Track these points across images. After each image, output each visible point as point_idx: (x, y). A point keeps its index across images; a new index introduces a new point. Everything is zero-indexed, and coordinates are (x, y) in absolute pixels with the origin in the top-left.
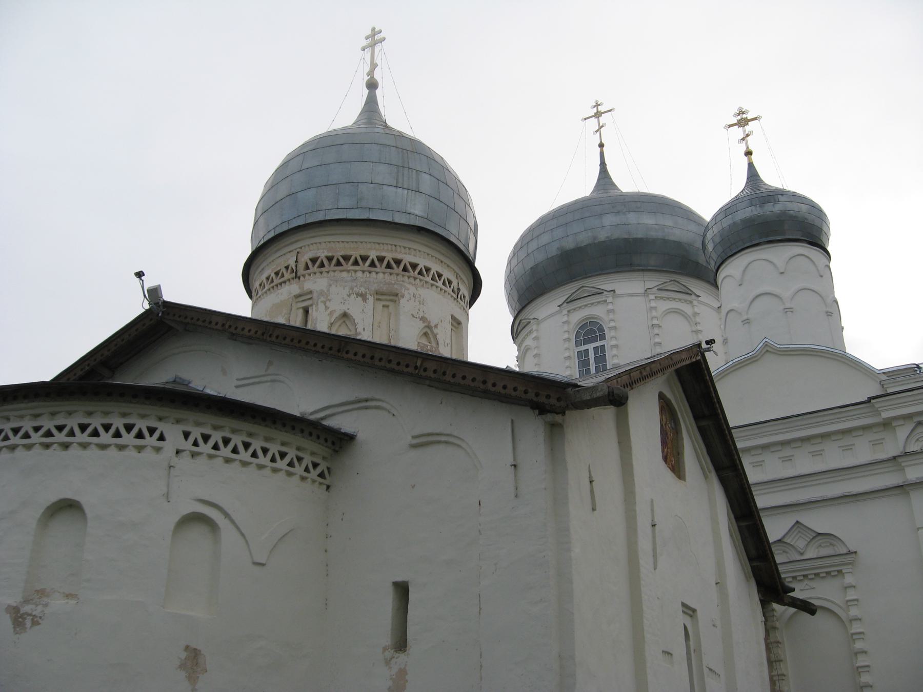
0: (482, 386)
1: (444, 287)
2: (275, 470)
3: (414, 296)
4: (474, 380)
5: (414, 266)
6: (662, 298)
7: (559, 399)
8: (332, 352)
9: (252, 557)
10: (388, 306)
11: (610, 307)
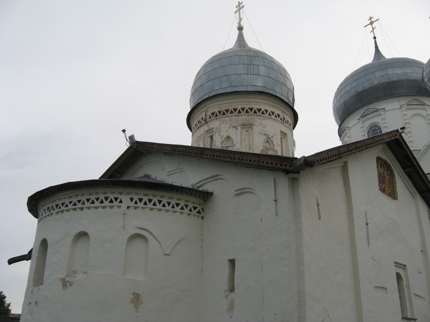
0: (258, 164)
1: (275, 118)
2: (175, 212)
3: (260, 124)
4: (254, 161)
5: (259, 110)
6: (409, 109)
7: (291, 166)
8: (198, 155)
9: (163, 252)
10: (248, 131)
11: (383, 117)
